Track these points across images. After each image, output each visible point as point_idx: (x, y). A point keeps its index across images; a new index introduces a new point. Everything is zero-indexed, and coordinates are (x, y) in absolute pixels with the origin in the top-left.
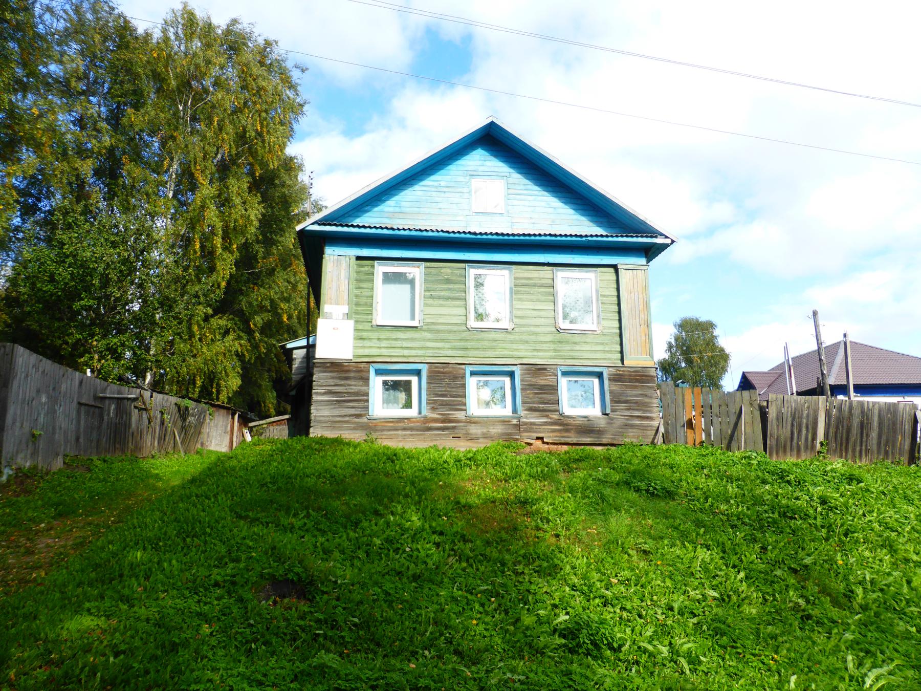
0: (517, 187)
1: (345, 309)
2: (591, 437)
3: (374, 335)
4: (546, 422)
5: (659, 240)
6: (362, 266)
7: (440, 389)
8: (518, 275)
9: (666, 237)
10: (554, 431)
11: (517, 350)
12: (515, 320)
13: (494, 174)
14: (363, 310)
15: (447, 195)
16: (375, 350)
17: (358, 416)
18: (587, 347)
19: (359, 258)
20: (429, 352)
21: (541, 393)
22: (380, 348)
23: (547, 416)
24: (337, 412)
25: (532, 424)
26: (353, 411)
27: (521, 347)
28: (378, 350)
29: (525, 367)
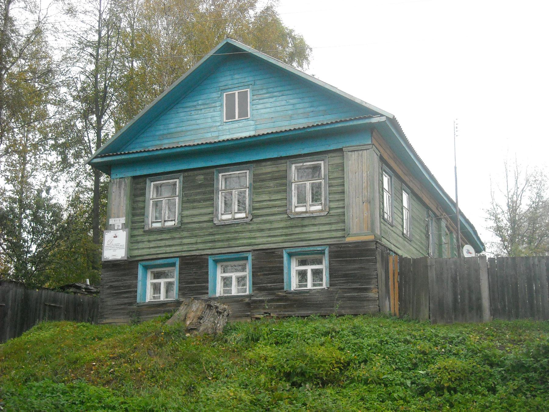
0: (261, 92)
1: (123, 220)
3: (146, 238)
6: (137, 184)
7: (189, 277)
8: (257, 172)
9: (382, 115)
10: (279, 307)
11: (254, 238)
13: (242, 84)
14: (140, 219)
15: (203, 111)
16: (143, 250)
17: (131, 304)
18: (315, 229)
19: (134, 178)
20: (185, 248)
21: (269, 274)
22: (150, 248)
23: (274, 294)
24: (116, 302)
26: (126, 301)
27: (258, 234)
28: (148, 250)
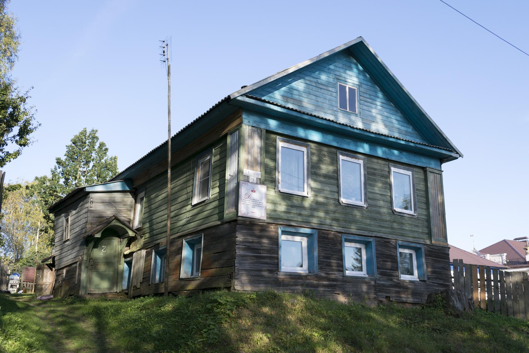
0: (365, 95)
2: (283, 222)
4: (391, 285)
5: (454, 155)
12: (368, 201)
15: (322, 91)
25: (383, 285)
29: (378, 239)
